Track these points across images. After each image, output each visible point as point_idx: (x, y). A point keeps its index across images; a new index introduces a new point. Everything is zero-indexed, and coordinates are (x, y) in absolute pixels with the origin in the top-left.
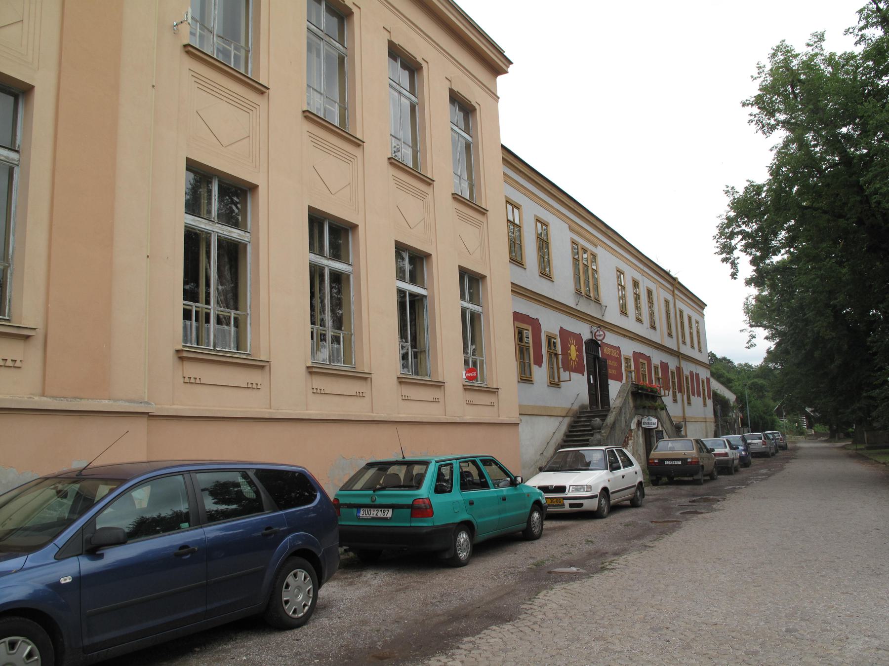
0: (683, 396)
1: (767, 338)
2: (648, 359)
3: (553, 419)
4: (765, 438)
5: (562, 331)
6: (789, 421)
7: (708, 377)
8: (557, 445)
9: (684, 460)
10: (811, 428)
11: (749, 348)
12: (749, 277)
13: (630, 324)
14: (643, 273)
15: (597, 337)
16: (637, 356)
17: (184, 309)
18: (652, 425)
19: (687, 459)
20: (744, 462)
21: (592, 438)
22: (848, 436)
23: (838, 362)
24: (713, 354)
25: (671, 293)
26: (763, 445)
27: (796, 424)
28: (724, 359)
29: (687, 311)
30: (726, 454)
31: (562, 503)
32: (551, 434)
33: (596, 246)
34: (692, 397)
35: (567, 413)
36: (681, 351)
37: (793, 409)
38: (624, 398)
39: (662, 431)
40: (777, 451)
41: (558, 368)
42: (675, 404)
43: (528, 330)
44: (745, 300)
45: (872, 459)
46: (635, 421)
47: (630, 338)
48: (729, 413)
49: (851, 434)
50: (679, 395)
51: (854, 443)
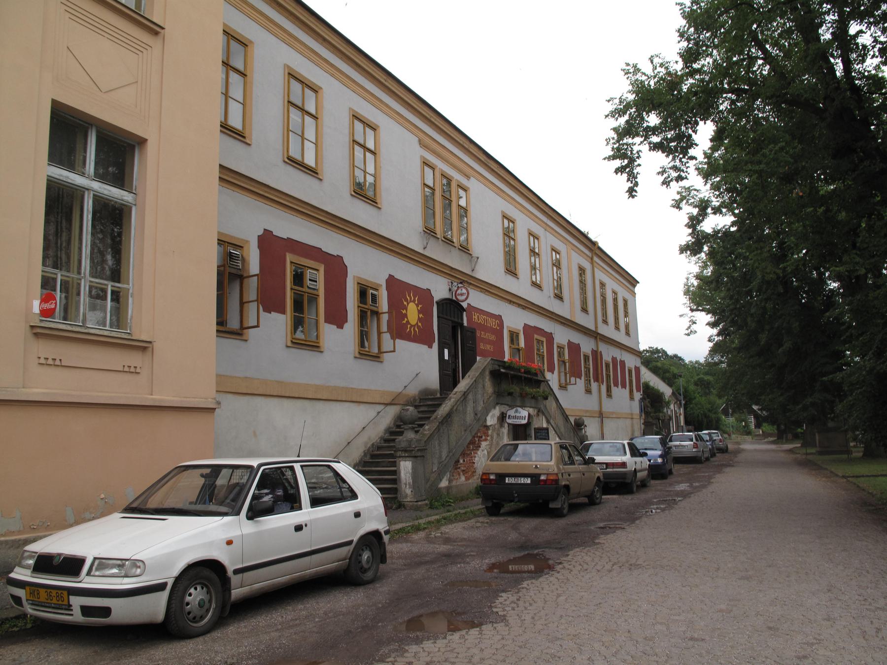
0: (600, 386)
1: (708, 324)
2: (550, 337)
3: (362, 407)
4: (697, 440)
5: (526, 327)
6: (737, 420)
7: (637, 366)
8: (369, 445)
9: (535, 477)
10: (760, 428)
11: (688, 335)
12: (684, 243)
13: (520, 287)
14: (546, 227)
15: (458, 297)
16: (529, 330)
17: (43, 277)
18: (521, 420)
19: (540, 475)
20: (657, 472)
21: (401, 437)
22: (796, 437)
23: (787, 345)
24: (664, 351)
25: (590, 260)
26: (694, 448)
27: (743, 423)
28: (676, 356)
29: (611, 285)
30: (624, 465)
31: (66, 603)
32: (359, 429)
33: (468, 177)
34: (614, 389)
35: (393, 400)
36: (600, 331)
37: (738, 407)
38: (474, 379)
39: (547, 429)
40: (713, 455)
41: (379, 333)
42: (589, 395)
43: (317, 270)
44: (686, 280)
45: (826, 469)
46: (496, 412)
47: (519, 305)
48: (663, 408)
49: (800, 435)
50: (594, 386)
51: (804, 445)
